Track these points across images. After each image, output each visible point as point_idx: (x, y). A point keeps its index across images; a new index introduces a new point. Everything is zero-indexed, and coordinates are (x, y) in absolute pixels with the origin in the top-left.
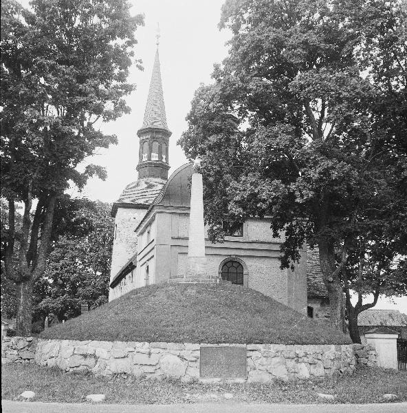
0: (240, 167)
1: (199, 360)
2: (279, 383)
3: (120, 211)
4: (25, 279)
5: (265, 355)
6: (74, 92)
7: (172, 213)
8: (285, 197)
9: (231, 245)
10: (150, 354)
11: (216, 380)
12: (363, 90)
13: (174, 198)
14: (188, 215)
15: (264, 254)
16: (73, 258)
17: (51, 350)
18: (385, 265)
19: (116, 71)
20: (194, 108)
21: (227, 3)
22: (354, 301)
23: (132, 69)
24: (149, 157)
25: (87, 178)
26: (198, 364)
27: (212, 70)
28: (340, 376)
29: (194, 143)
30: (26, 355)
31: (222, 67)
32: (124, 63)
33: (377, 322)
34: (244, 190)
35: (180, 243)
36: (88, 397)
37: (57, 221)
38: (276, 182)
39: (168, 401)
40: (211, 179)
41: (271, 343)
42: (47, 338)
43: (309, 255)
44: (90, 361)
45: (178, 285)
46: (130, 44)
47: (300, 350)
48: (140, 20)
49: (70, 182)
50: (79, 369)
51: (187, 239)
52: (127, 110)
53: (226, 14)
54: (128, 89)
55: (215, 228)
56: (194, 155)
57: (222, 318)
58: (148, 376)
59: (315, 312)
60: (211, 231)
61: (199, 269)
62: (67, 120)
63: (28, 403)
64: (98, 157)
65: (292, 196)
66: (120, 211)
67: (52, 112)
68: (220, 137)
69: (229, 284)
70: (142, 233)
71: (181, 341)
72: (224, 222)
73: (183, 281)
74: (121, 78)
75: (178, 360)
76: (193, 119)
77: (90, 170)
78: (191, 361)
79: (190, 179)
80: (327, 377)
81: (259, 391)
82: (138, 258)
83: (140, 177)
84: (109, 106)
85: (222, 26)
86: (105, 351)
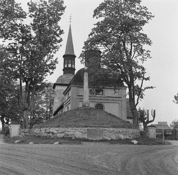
7: (78, 87)
24: (68, 66)
26: (86, 134)
82: (64, 104)
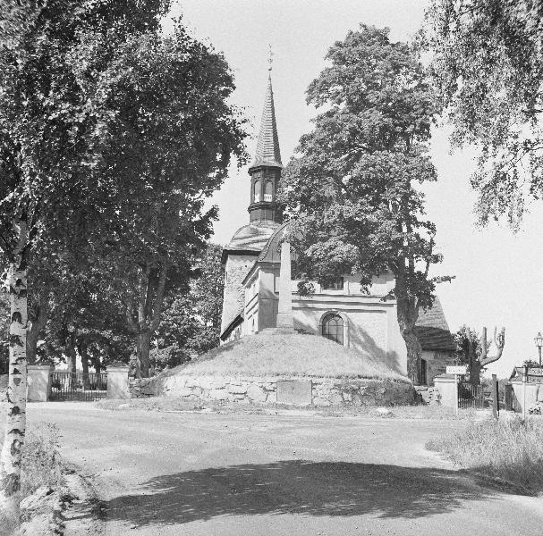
70: (249, 286)
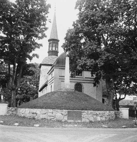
0: (81, 54)
1: (67, 115)
2: (91, 122)
3: (42, 66)
4: (13, 89)
5: (87, 114)
6: (29, 31)
8: (94, 64)
9: (78, 78)
10: (53, 113)
11: (72, 121)
12: (120, 31)
13: (60, 63)
14: (65, 69)
15: (88, 82)
16: (26, 82)
17: (23, 111)
18: (128, 85)
19: (42, 23)
20: (67, 36)
21: (78, 1)
22: (118, 98)
23: (47, 22)
25: (33, 57)
26: (67, 116)
27: (73, 23)
28: (110, 120)
29: (66, 46)
30: (14, 113)
31: (76, 23)
32: (45, 20)
33: (126, 104)
34: (82, 62)
35: (62, 78)
36: (34, 125)
37: (23, 70)
38: (93, 60)
39: (58, 127)
40: (72, 58)
41: (89, 110)
42: (21, 108)
43: (103, 83)
44: (35, 115)
45: (61, 92)
46: (46, 14)
47: (98, 112)
48: (49, 6)
49: (27, 58)
50: (31, 117)
51: (64, 77)
52: (46, 37)
53: (77, 5)
54: (46, 29)
55: (73, 73)
56: (67, 50)
57: (73, 103)
58: (52, 120)
59: (105, 100)
60: (72, 74)
61: (68, 87)
62: (27, 39)
63: (17, 127)
64: (36, 51)
65: (97, 64)
66: (42, 66)
67: (22, 37)
68: (75, 44)
69: (77, 92)
70: (50, 74)
71: (62, 109)
72: (76, 71)
73: (63, 91)
74: (44, 25)
75: (61, 115)
76: (66, 39)
77: (34, 55)
78: (65, 115)
79: (65, 58)
80: (106, 120)
81: (85, 124)
82: (48, 82)
83: (49, 55)
84: (40, 35)
85: (76, 8)
86: (39, 112)
